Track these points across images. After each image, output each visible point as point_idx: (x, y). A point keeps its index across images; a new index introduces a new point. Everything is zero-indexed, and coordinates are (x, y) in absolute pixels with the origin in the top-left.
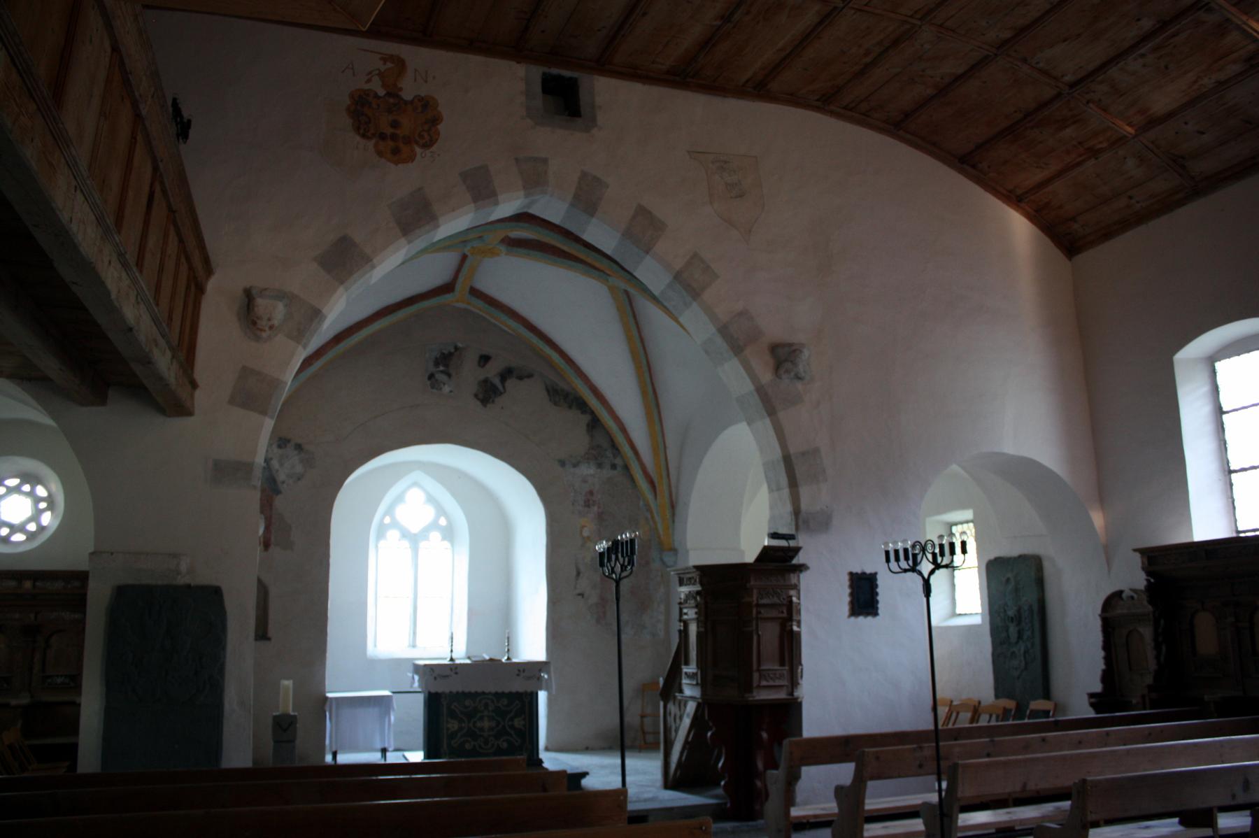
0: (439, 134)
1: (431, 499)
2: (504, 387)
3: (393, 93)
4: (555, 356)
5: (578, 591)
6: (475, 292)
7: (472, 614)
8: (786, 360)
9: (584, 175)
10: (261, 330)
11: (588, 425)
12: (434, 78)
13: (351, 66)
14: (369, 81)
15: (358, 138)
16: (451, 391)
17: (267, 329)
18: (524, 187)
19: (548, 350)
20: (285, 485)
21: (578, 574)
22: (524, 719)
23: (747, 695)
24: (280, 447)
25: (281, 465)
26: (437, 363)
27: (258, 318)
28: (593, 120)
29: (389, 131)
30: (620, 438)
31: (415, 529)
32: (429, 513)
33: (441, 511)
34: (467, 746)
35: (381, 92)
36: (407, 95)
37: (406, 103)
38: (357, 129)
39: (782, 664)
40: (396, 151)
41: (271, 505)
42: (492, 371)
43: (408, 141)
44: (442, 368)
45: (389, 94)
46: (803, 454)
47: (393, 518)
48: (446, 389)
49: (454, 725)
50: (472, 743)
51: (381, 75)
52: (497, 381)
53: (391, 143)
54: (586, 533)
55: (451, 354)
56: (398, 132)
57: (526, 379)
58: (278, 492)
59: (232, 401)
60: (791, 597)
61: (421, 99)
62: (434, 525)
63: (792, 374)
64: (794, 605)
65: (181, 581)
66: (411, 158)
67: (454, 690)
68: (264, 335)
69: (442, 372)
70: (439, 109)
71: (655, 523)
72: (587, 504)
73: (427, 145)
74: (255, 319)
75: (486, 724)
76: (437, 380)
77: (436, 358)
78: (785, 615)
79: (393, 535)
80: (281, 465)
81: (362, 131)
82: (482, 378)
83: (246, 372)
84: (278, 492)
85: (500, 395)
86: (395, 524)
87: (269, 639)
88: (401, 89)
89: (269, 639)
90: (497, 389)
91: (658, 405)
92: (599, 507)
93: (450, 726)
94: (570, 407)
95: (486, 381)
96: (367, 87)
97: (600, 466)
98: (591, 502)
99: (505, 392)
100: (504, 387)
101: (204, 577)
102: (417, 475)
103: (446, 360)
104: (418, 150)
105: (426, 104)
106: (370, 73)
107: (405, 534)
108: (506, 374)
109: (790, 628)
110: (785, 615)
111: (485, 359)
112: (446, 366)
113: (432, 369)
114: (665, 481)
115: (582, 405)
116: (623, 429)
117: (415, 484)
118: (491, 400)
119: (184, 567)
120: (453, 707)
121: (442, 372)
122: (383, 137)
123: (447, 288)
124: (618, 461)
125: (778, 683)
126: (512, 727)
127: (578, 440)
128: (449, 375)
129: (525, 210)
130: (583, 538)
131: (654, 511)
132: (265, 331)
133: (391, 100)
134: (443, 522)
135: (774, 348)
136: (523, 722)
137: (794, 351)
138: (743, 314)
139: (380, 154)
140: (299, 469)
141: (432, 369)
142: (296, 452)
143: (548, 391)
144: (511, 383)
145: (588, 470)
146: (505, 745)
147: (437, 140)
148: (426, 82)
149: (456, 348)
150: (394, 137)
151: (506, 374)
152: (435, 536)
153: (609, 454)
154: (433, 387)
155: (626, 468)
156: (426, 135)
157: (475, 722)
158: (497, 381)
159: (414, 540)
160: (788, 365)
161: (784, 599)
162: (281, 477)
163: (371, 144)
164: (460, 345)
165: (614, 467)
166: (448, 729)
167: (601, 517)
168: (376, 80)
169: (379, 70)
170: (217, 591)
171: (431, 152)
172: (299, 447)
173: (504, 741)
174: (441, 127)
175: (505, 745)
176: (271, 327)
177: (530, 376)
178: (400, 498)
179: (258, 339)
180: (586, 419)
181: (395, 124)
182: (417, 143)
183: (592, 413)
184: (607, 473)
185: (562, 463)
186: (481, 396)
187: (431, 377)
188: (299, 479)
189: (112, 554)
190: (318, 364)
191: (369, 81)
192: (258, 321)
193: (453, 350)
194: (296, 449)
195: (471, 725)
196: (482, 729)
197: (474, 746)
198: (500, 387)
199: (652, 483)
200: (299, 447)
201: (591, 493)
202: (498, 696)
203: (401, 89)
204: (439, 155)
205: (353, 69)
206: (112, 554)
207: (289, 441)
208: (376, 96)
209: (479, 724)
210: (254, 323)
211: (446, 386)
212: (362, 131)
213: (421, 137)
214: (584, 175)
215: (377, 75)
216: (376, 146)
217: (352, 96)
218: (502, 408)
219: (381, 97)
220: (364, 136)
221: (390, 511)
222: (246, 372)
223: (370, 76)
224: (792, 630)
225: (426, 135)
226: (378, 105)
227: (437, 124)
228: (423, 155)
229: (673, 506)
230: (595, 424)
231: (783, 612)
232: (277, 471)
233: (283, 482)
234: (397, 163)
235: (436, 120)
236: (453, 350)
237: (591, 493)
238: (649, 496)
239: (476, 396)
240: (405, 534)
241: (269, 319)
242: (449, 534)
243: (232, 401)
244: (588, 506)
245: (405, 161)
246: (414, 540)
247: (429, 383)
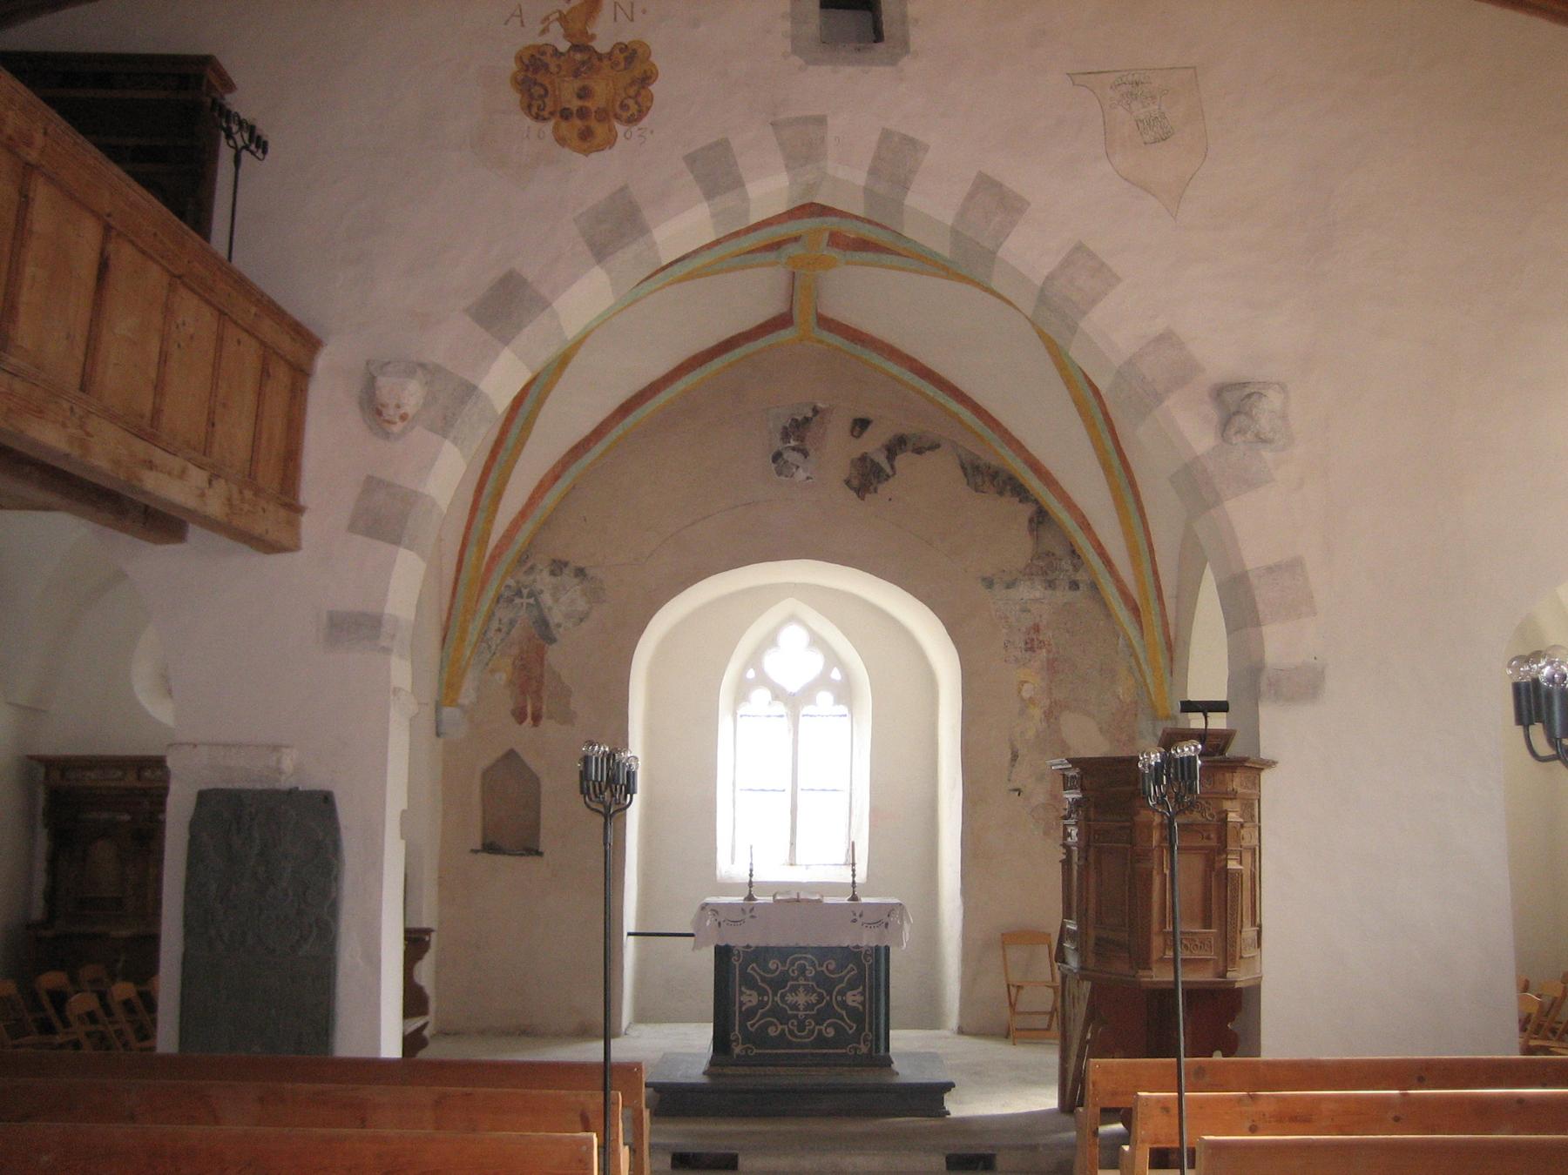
0: (652, 100)
1: (817, 641)
2: (892, 467)
3: (581, 45)
4: (966, 414)
5: (1012, 786)
6: (826, 323)
7: (875, 814)
8: (1238, 412)
9: (886, 135)
10: (389, 422)
11: (1031, 521)
12: (644, 12)
13: (518, 12)
14: (544, 31)
15: (529, 121)
16: (808, 478)
17: (397, 420)
18: (787, 166)
19: (954, 406)
20: (561, 630)
21: (1015, 757)
22: (863, 994)
23: (1141, 973)
24: (553, 573)
25: (556, 600)
26: (786, 435)
27: (382, 405)
28: (905, 45)
29: (575, 104)
30: (1081, 540)
31: (793, 685)
32: (815, 663)
33: (833, 658)
34: (772, 1032)
35: (564, 46)
36: (602, 45)
37: (600, 57)
38: (528, 109)
39: (1207, 924)
40: (586, 135)
41: (542, 659)
42: (872, 443)
43: (604, 115)
44: (793, 443)
45: (575, 47)
46: (1270, 570)
47: (761, 673)
48: (801, 475)
49: (749, 998)
50: (780, 1027)
51: (563, 19)
52: (881, 459)
53: (578, 123)
54: (1027, 692)
55: (807, 420)
56: (588, 104)
57: (928, 453)
58: (552, 640)
59: (352, 527)
60: (1226, 812)
61: (623, 48)
62: (822, 681)
63: (1249, 436)
64: (1230, 825)
65: (285, 783)
66: (610, 142)
67: (753, 944)
68: (396, 429)
69: (794, 449)
70: (652, 59)
71: (1142, 675)
72: (1030, 647)
73: (632, 120)
74: (380, 407)
75: (801, 999)
76: (786, 462)
77: (785, 428)
78: (1213, 843)
79: (761, 696)
80: (556, 600)
81: (534, 110)
82: (857, 455)
83: (372, 484)
84: (552, 640)
85: (886, 480)
86: (763, 680)
87: (539, 854)
88: (593, 37)
89: (539, 854)
90: (881, 470)
91: (1133, 484)
92: (1049, 652)
93: (744, 998)
94: (1001, 493)
95: (864, 458)
96: (541, 41)
97: (1051, 585)
98: (1036, 643)
99: (894, 473)
100: (892, 467)
101: (315, 780)
102: (789, 605)
103: (799, 430)
104: (620, 128)
105: (631, 56)
106: (547, 18)
107: (778, 694)
108: (896, 446)
109: (1223, 863)
110: (1213, 843)
111: (861, 425)
112: (801, 439)
113: (778, 445)
114: (1154, 606)
115: (1020, 491)
116: (1085, 526)
117: (792, 618)
118: (872, 488)
119: (288, 764)
120: (749, 970)
121: (794, 449)
122: (565, 115)
123: (781, 322)
124: (1081, 576)
125: (1198, 954)
126: (844, 1005)
127: (1016, 545)
128: (805, 454)
129: (805, 201)
130: (1023, 699)
131: (1141, 656)
132: (395, 423)
133: (578, 56)
134: (836, 675)
135: (1219, 392)
136: (859, 998)
137: (1249, 396)
138: (1166, 338)
139: (561, 141)
140: (581, 605)
141: (778, 445)
142: (576, 580)
143: (963, 468)
144: (903, 460)
145: (1032, 591)
146: (831, 1033)
147: (648, 109)
148: (632, 20)
149: (816, 411)
150: (583, 113)
151: (896, 446)
152: (825, 698)
153: (1066, 564)
154: (779, 473)
155: (1094, 587)
156: (631, 102)
157: (783, 996)
158: (881, 459)
159: (794, 702)
160: (1241, 420)
161: (1211, 815)
162: (555, 616)
163: (548, 127)
164: (820, 405)
165: (1074, 585)
166: (742, 1004)
167: (1052, 667)
168: (556, 29)
169: (560, 12)
170: (324, 803)
171: (639, 129)
172: (580, 572)
173: (828, 1026)
174: (654, 88)
175: (831, 1033)
176: (403, 417)
177: (935, 447)
178: (770, 640)
179: (387, 435)
180: (1027, 510)
181: (584, 94)
182: (617, 117)
183: (1036, 501)
184: (1062, 595)
185: (989, 583)
186: (855, 483)
187: (777, 457)
188: (581, 620)
189: (195, 746)
190: (1089, 394)
191: (544, 31)
192: (384, 411)
193: (810, 414)
194: (576, 576)
195: (777, 999)
196: (795, 1007)
197: (783, 1030)
198: (888, 470)
199: (1135, 610)
200: (580, 572)
201: (1037, 629)
202: (824, 953)
203: (593, 37)
204: (652, 132)
205: (521, 16)
206: (195, 746)
207: (566, 564)
208: (556, 53)
209: (790, 998)
210: (379, 413)
211: (801, 470)
212: (534, 110)
213: (624, 106)
214: (886, 135)
215: (557, 19)
216: (556, 129)
217: (519, 58)
218: (890, 499)
219: (561, 54)
220: (537, 118)
221: (755, 659)
222: (372, 484)
223: (547, 23)
224: (1225, 869)
225: (631, 102)
226: (559, 66)
227: (649, 85)
228: (628, 136)
229: (1170, 647)
230: (1041, 517)
231: (1208, 838)
232: (550, 609)
233: (559, 625)
234: (586, 152)
235: (647, 78)
236: (810, 414)
237: (1037, 629)
238: (1132, 631)
239: (848, 482)
240: (778, 694)
241: (398, 406)
242: (845, 693)
243: (352, 527)
244: (1032, 649)
245: (599, 148)
246: (794, 702)
247: (773, 466)
